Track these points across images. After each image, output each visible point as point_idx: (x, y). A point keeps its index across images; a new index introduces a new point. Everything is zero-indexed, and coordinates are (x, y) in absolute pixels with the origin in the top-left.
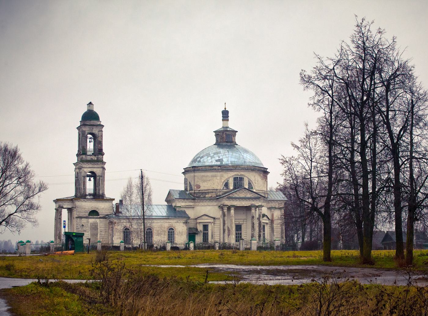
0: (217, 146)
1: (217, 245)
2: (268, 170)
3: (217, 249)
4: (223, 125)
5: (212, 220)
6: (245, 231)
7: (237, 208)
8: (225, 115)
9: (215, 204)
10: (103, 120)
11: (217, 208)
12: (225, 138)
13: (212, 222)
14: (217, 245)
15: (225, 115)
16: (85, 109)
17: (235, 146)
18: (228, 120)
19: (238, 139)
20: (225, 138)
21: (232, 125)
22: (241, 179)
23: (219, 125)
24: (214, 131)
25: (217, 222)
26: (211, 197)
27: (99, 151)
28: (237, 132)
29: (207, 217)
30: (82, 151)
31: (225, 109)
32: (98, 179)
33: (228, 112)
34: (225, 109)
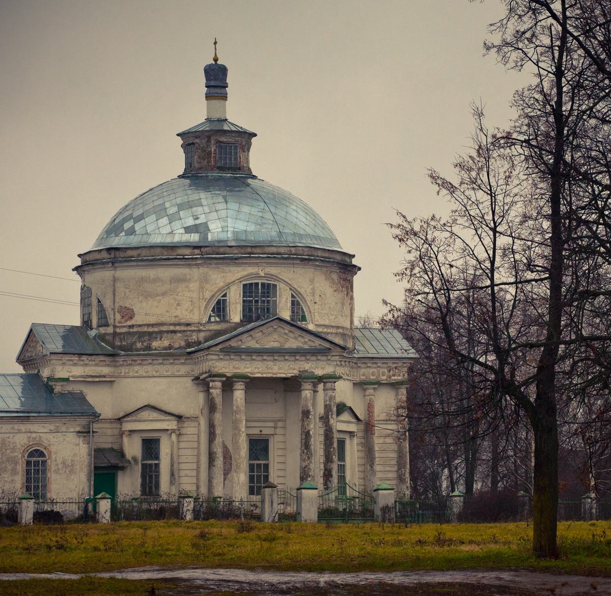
0: (187, 181)
1: (188, 506)
2: (355, 262)
5: (172, 424)
7: (253, 384)
8: (216, 79)
9: (184, 369)
11: (188, 382)
12: (217, 157)
13: (173, 431)
14: (188, 506)
15: (216, 79)
19: (258, 160)
20: (217, 157)
21: (237, 113)
22: (269, 289)
23: (196, 113)
24: (177, 133)
25: (190, 429)
26: (170, 347)
28: (255, 135)
29: (154, 415)
31: (216, 60)
33: (223, 70)
34: (216, 60)
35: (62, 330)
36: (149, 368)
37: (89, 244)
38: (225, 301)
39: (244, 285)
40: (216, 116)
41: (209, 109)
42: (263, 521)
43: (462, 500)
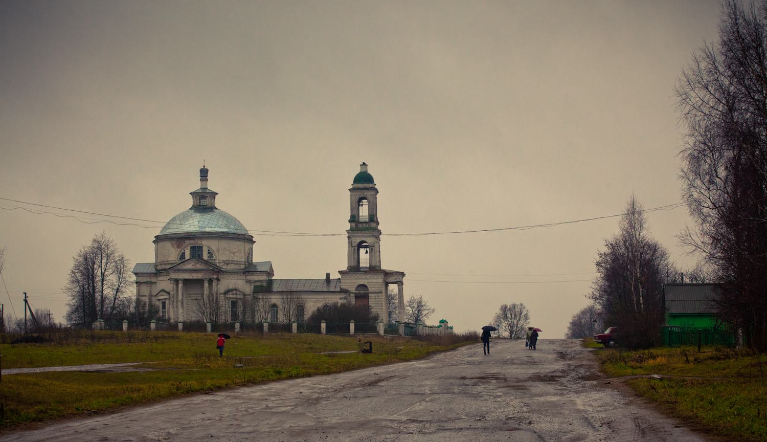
0: (193, 210)
1: (180, 326)
2: (254, 240)
3: (382, 332)
4: (201, 186)
6: (188, 311)
7: (186, 282)
8: (204, 173)
10: (378, 183)
12: (204, 201)
14: (180, 326)
15: (204, 173)
16: (357, 170)
17: (214, 210)
18: (207, 180)
19: (218, 203)
20: (204, 201)
21: (211, 186)
22: (201, 248)
23: (197, 186)
24: (191, 192)
27: (373, 218)
28: (218, 194)
29: (164, 293)
30: (354, 219)
31: (204, 167)
32: (374, 250)
33: (207, 171)
34: (204, 167)
35: (378, 264)
36: (367, 276)
37: (158, 232)
38: (184, 253)
39: (191, 247)
40: (203, 187)
41: (201, 185)
42: (292, 332)
43: (493, 332)
